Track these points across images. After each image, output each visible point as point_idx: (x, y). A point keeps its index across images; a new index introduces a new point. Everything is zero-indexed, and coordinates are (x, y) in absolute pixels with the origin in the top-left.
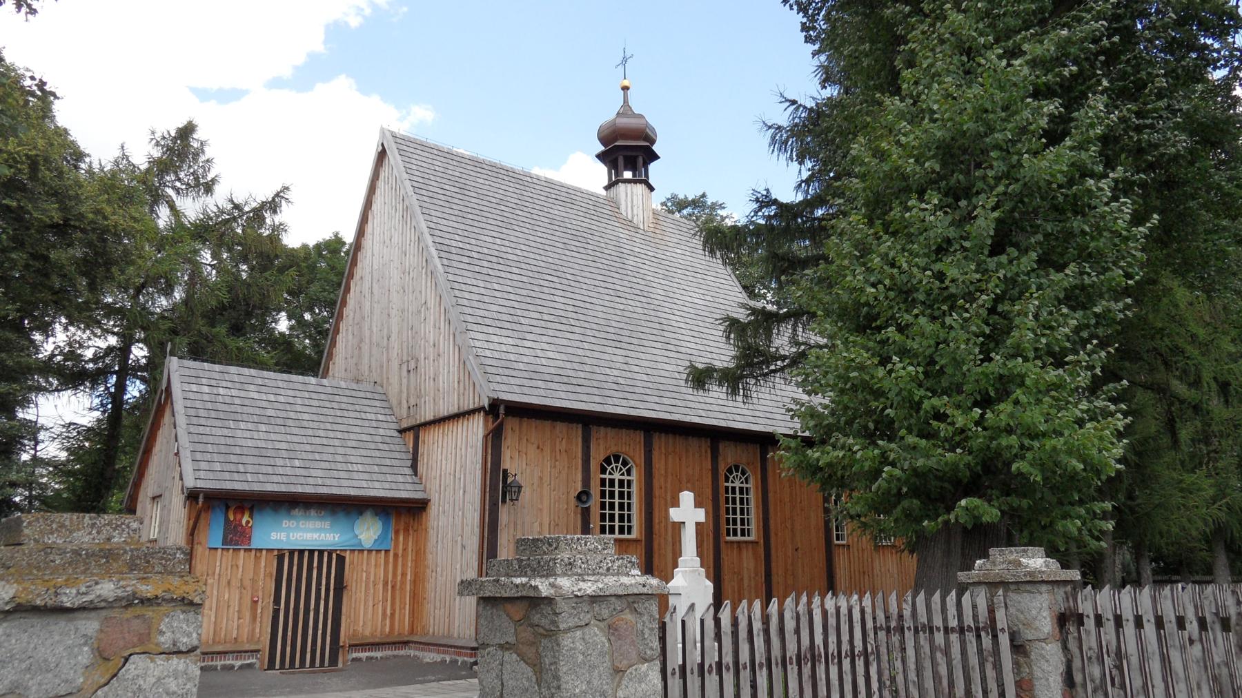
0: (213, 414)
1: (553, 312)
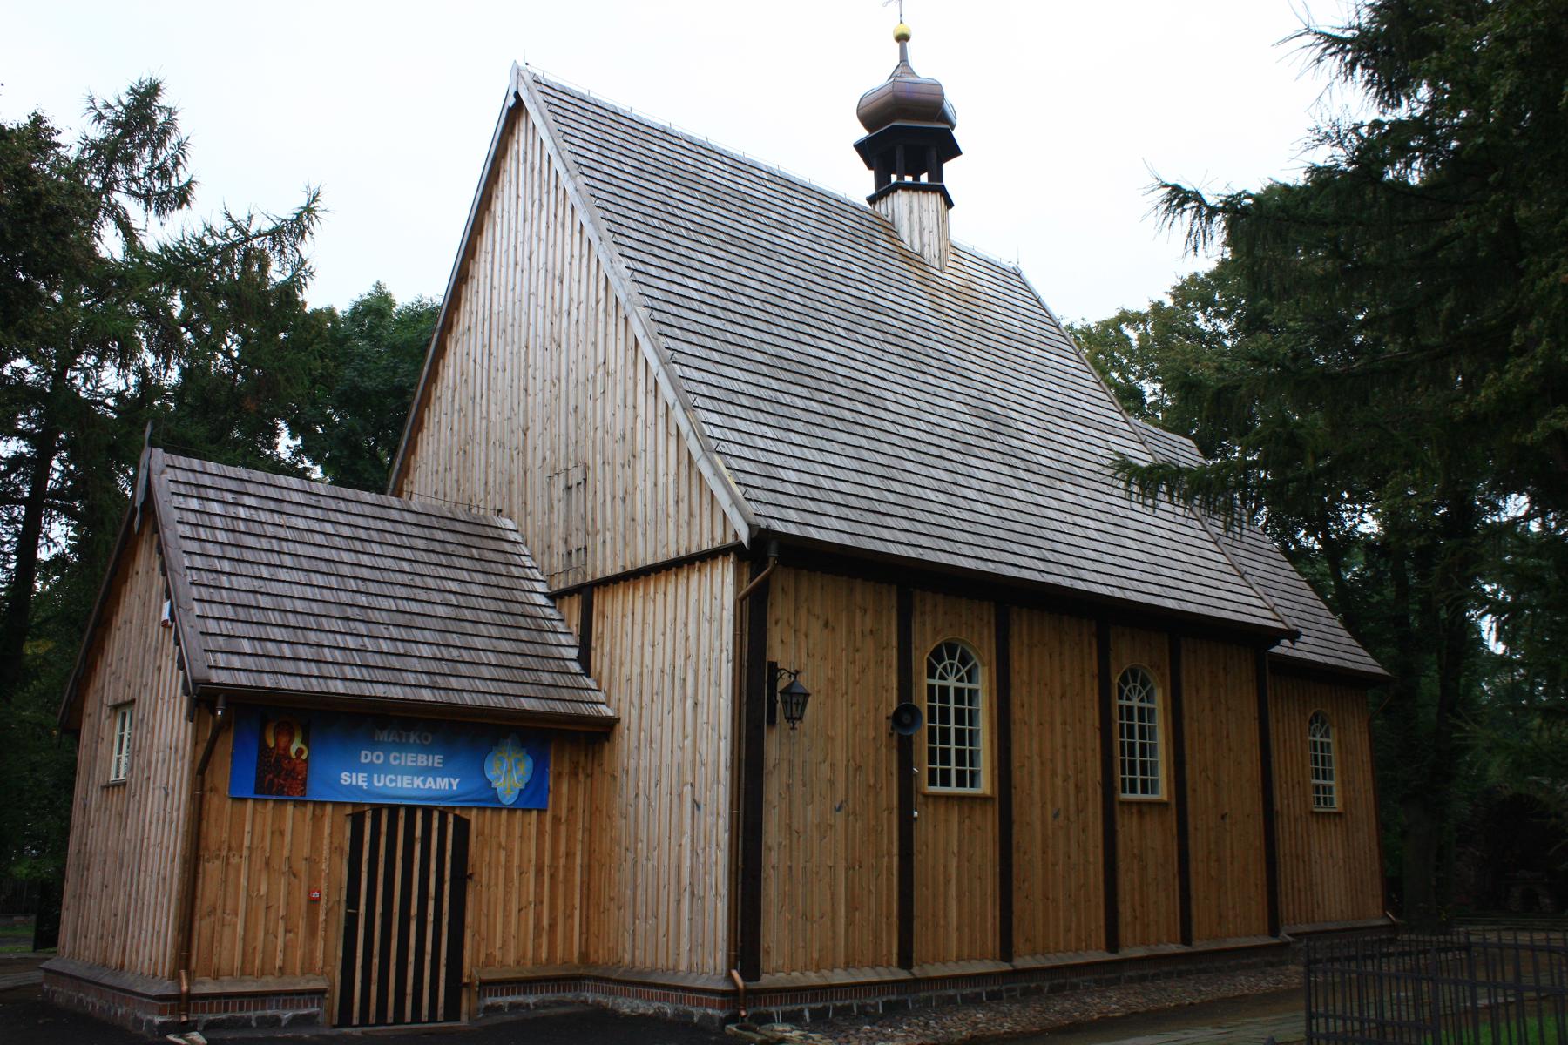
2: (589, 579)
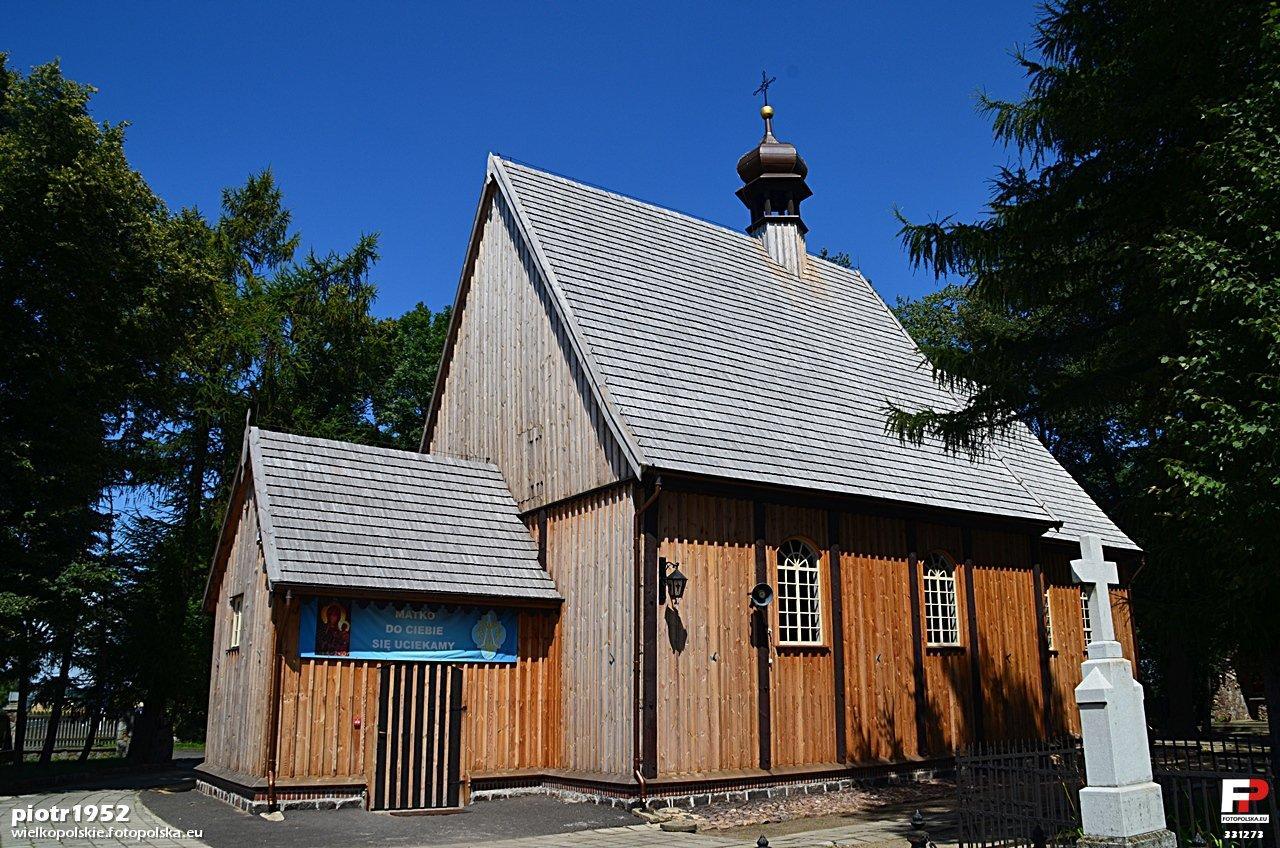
0: (300, 494)
1: (706, 364)
2: (545, 504)
